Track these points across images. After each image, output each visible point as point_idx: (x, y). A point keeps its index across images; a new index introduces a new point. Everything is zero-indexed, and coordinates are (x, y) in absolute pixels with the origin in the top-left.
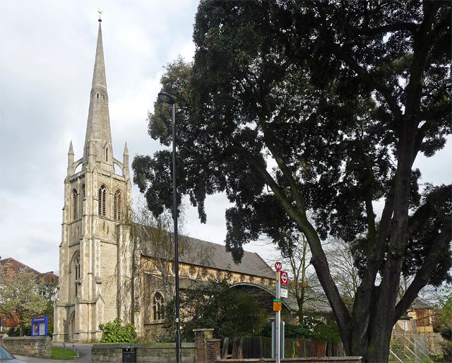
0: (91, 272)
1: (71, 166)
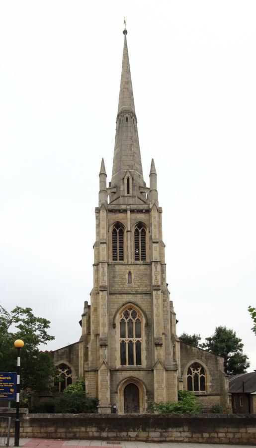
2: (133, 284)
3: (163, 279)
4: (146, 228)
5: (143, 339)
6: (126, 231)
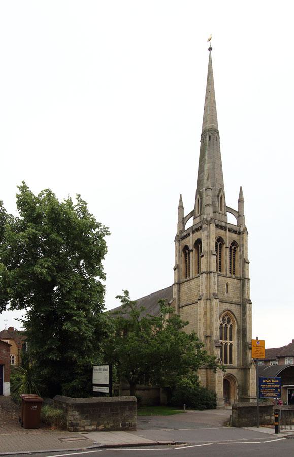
0: (208, 334)
1: (183, 221)
3: (249, 296)
4: (237, 247)
5: (235, 342)
6: (224, 247)
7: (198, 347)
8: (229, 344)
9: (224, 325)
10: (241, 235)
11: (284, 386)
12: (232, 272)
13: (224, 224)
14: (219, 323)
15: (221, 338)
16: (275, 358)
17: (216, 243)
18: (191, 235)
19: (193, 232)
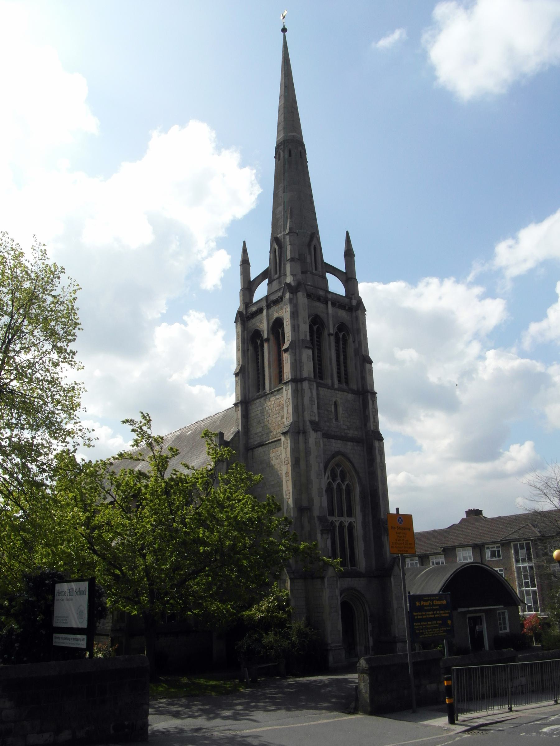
0: (305, 504)
2: (342, 423)
4: (348, 335)
5: (357, 520)
6: (326, 333)
7: (154, 485)
8: (347, 524)
9: (335, 486)
10: (354, 314)
11: (460, 610)
12: (343, 380)
13: (321, 293)
14: (324, 481)
15: (331, 513)
16: (440, 550)
17: (311, 327)
18: (265, 312)
19: (268, 307)
